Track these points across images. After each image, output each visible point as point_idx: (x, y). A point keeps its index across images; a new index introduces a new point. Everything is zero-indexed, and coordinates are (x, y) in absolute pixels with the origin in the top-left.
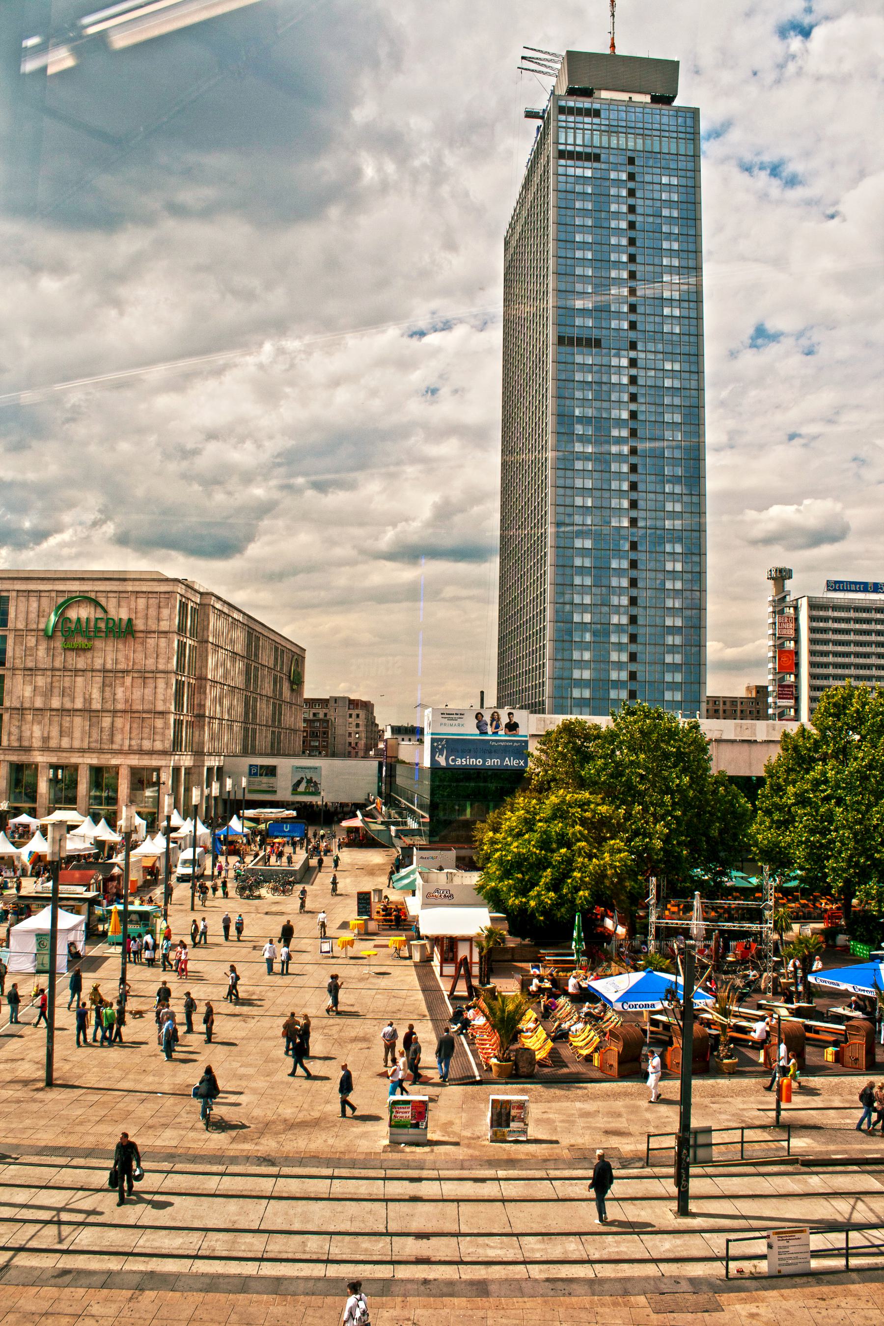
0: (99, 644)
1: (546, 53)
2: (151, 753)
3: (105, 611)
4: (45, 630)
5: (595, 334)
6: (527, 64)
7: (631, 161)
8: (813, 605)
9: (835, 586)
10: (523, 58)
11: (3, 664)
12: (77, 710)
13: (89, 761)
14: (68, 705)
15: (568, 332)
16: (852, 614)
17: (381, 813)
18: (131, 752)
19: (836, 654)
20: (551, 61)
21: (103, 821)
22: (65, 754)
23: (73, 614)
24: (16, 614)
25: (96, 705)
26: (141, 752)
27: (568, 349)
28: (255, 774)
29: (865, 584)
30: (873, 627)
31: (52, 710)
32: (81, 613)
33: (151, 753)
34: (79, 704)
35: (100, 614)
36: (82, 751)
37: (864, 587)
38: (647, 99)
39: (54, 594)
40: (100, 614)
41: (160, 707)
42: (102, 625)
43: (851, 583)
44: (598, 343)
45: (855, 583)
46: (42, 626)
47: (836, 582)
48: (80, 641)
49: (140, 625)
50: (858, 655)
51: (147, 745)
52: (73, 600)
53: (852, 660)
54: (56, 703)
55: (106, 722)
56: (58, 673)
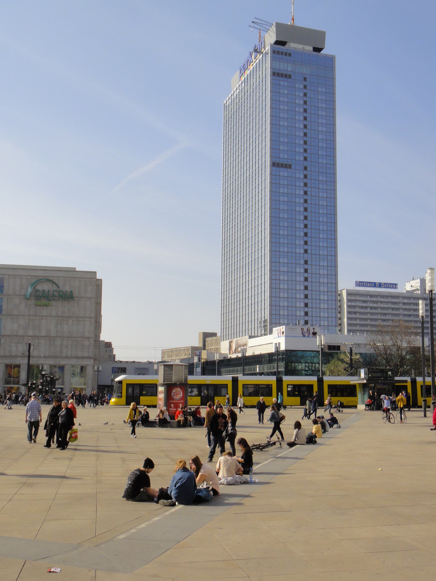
0: (54, 303)
1: (259, 19)
2: (83, 358)
3: (58, 287)
4: (25, 296)
5: (289, 162)
6: (253, 25)
7: (305, 79)
8: (349, 294)
9: (360, 284)
10: (253, 22)
11: (1, 313)
12: (42, 337)
13: (49, 362)
14: (37, 334)
15: (277, 161)
16: (368, 298)
17: (57, 409)
18: (72, 357)
19: (361, 319)
20: (266, 25)
21: (284, 362)
22: (36, 359)
23: (40, 287)
24: (8, 287)
25: (53, 334)
26: (77, 358)
27: (278, 169)
28: (115, 372)
29: (375, 283)
30: (379, 305)
31: (29, 336)
32: (45, 287)
33: (83, 358)
34: (43, 333)
35: (55, 288)
36: (45, 357)
37: (374, 285)
38: (311, 49)
39: (29, 277)
40: (55, 288)
41: (87, 335)
42: (56, 294)
43: (368, 282)
44: (290, 166)
45: (370, 283)
46: (23, 293)
47: (360, 282)
48: (44, 302)
49: (76, 294)
50: (371, 320)
51: (80, 354)
52: (40, 281)
53: (369, 322)
54: (31, 333)
55: (58, 342)
56: (32, 318)
